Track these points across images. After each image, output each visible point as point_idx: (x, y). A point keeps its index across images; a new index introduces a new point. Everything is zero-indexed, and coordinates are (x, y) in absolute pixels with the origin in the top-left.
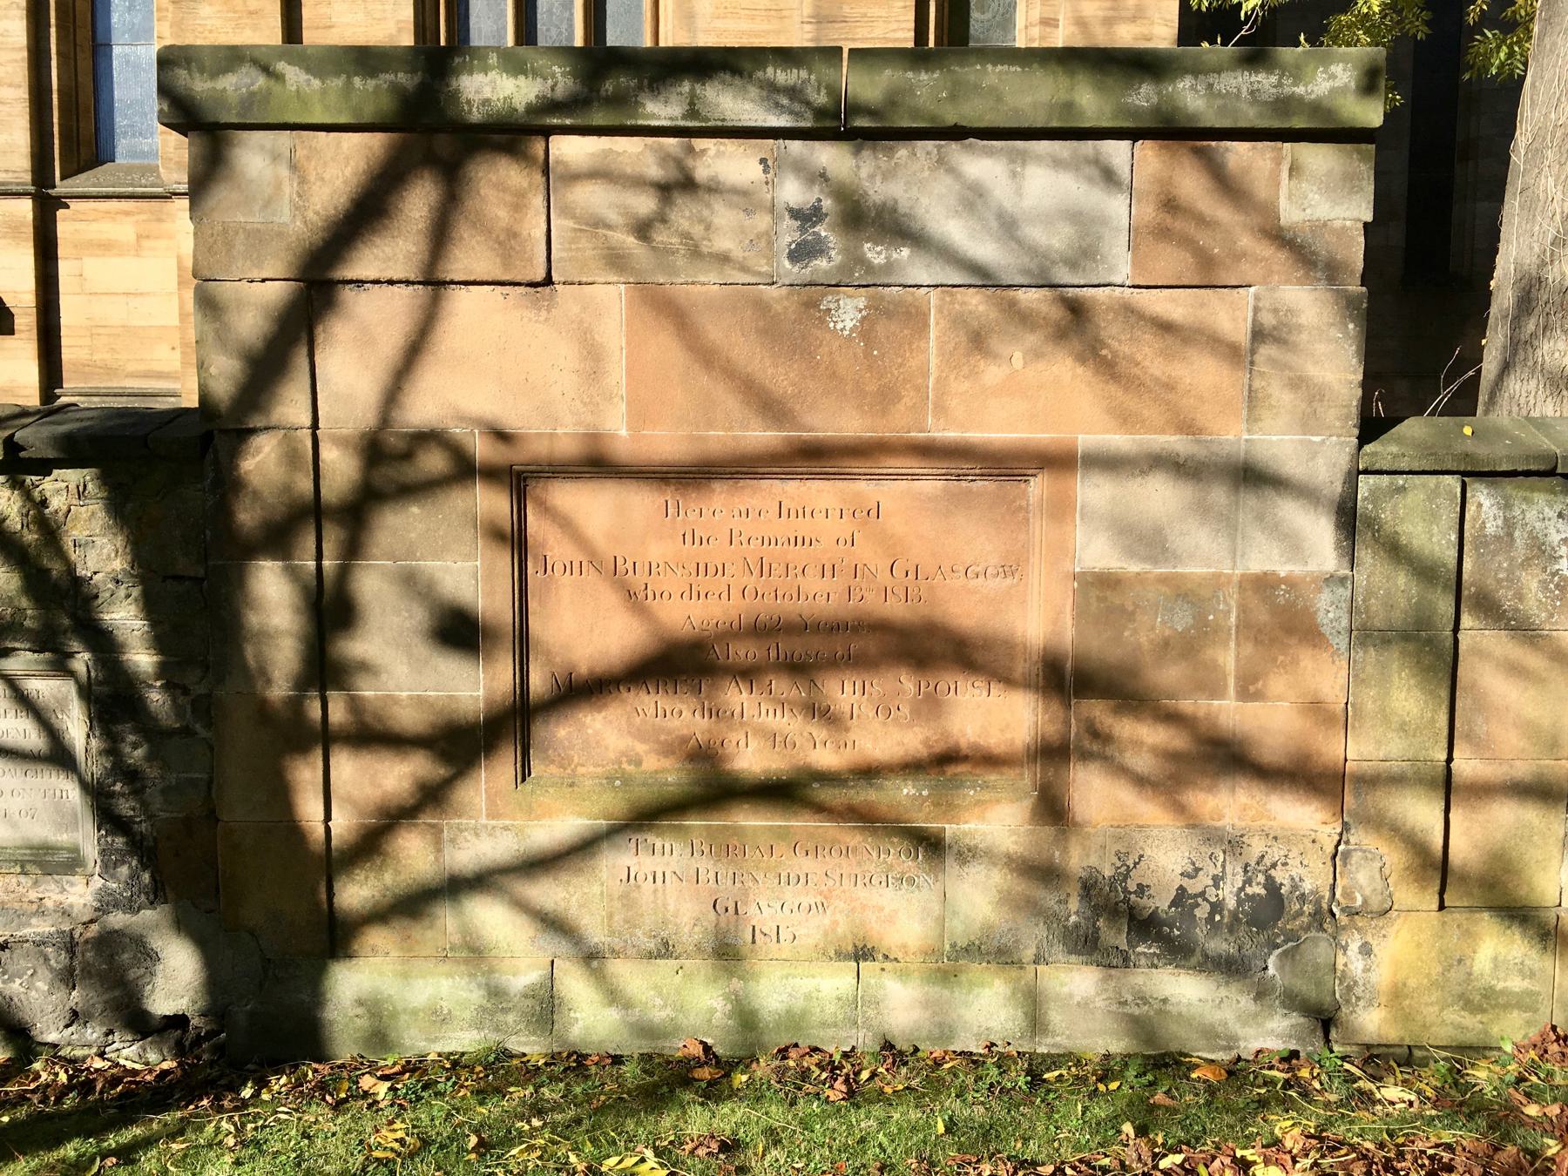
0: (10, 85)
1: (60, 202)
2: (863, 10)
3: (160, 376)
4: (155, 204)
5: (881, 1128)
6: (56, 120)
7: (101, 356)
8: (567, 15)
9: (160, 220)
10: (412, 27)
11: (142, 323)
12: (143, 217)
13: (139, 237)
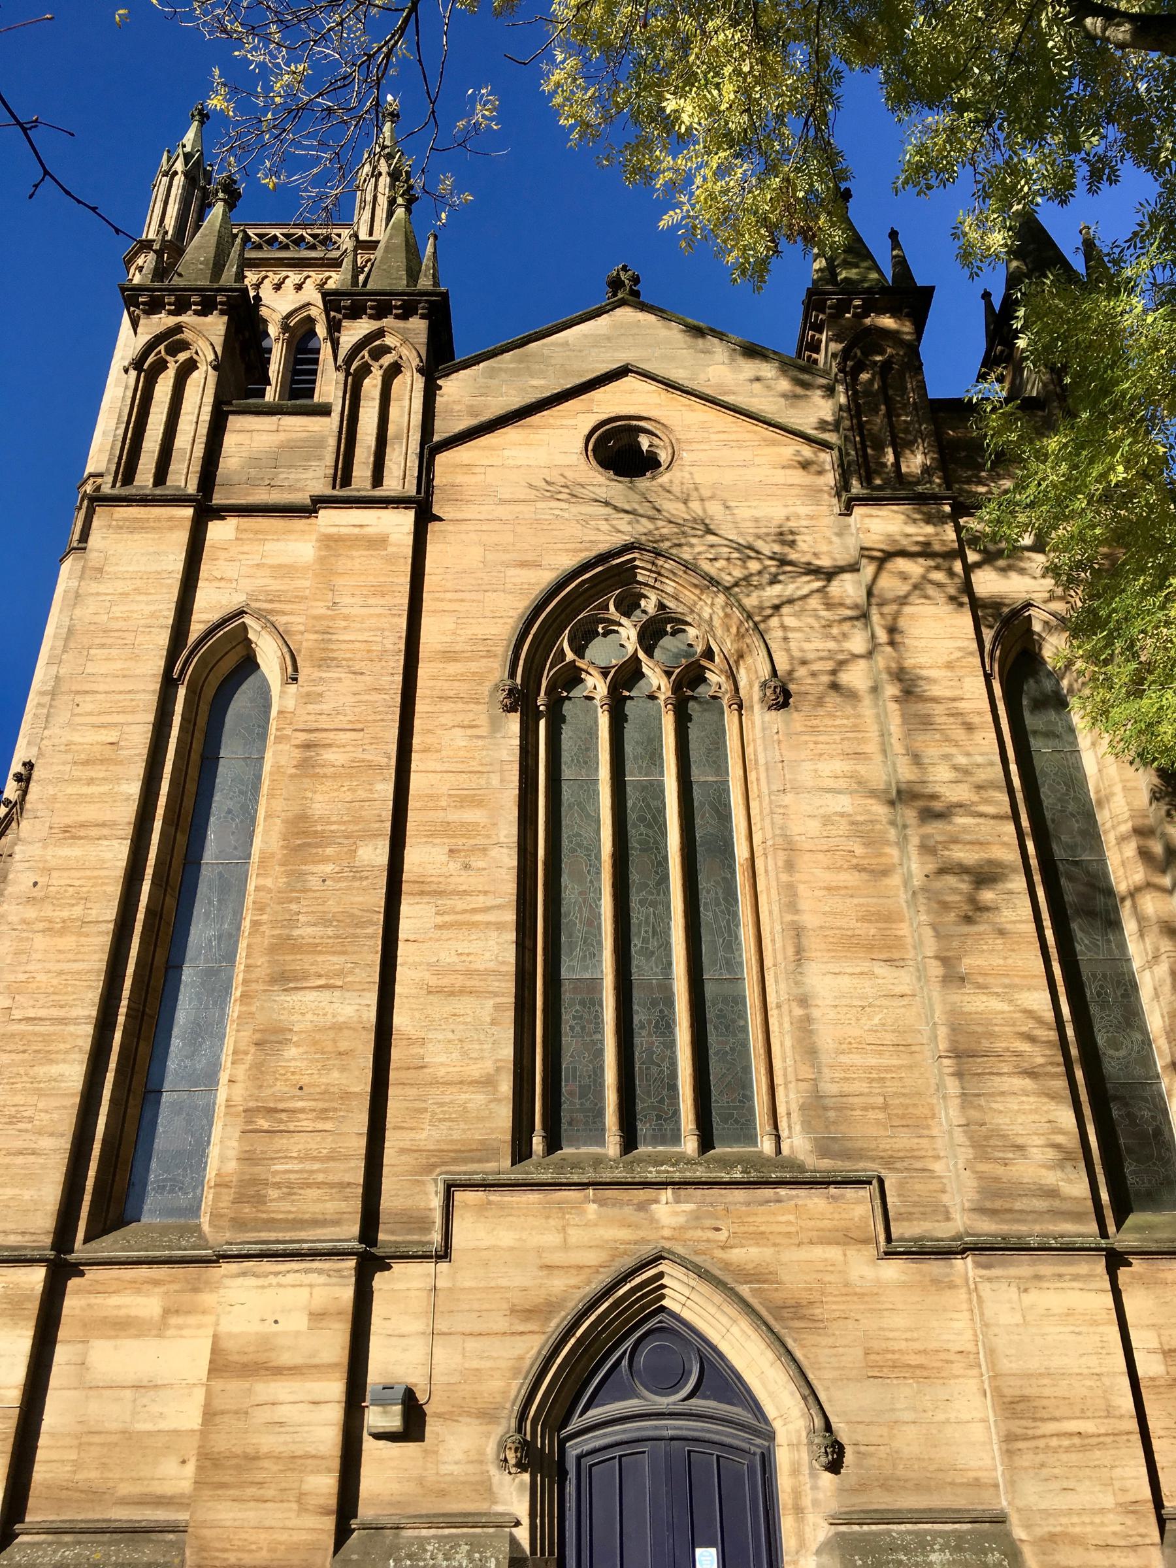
0: (52, 1135)
1: (76, 1270)
3: (160, 1501)
4: (192, 1271)
7: (90, 1475)
8: (668, 1053)
9: (196, 1290)
10: (511, 1066)
11: (149, 1427)
12: (176, 1287)
13: (167, 1312)
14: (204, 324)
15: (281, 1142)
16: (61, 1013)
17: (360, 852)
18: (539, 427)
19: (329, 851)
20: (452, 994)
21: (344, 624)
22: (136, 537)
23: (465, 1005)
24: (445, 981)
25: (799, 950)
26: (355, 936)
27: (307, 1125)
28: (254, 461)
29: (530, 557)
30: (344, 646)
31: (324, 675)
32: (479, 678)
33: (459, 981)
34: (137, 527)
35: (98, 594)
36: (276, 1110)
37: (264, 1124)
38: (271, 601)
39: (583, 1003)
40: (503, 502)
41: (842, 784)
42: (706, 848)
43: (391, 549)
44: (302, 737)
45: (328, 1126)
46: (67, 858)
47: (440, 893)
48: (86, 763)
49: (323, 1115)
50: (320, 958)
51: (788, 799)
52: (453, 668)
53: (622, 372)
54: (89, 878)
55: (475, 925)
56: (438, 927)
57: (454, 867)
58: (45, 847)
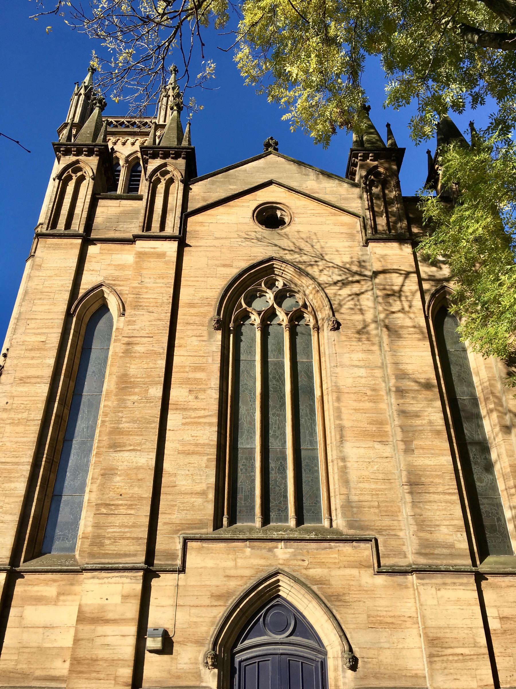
0: (11, 514)
2: (431, 480)
4: (70, 576)
5: (482, 368)
6: (28, 531)
7: (23, 666)
9: (72, 584)
12: (63, 583)
14: (89, 160)
15: (111, 519)
16: (17, 460)
17: (150, 391)
18: (233, 206)
19: (137, 390)
20: (189, 454)
21: (146, 290)
22: (56, 251)
23: (194, 459)
24: (186, 448)
25: (342, 437)
26: (147, 428)
27: (124, 512)
28: (109, 219)
29: (228, 262)
30: (145, 300)
31: (136, 313)
32: (204, 315)
33: (192, 448)
34: (57, 247)
35: (39, 276)
36: (110, 505)
37: (104, 511)
38: (114, 280)
39: (246, 459)
40: (217, 238)
41: (361, 363)
42: (302, 391)
43: (167, 258)
44: (126, 340)
45: (132, 512)
46: (22, 392)
47: (185, 409)
48: (31, 350)
49: (130, 507)
50: (131, 437)
51: (338, 370)
52: (193, 311)
53: (270, 183)
54: (31, 401)
55: (199, 423)
56: (183, 424)
57: (191, 398)
58: (12, 387)
